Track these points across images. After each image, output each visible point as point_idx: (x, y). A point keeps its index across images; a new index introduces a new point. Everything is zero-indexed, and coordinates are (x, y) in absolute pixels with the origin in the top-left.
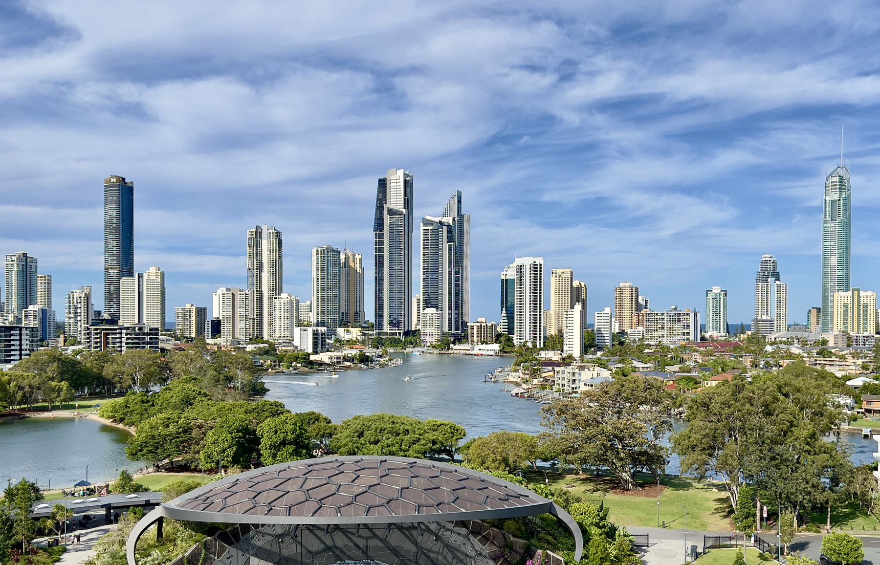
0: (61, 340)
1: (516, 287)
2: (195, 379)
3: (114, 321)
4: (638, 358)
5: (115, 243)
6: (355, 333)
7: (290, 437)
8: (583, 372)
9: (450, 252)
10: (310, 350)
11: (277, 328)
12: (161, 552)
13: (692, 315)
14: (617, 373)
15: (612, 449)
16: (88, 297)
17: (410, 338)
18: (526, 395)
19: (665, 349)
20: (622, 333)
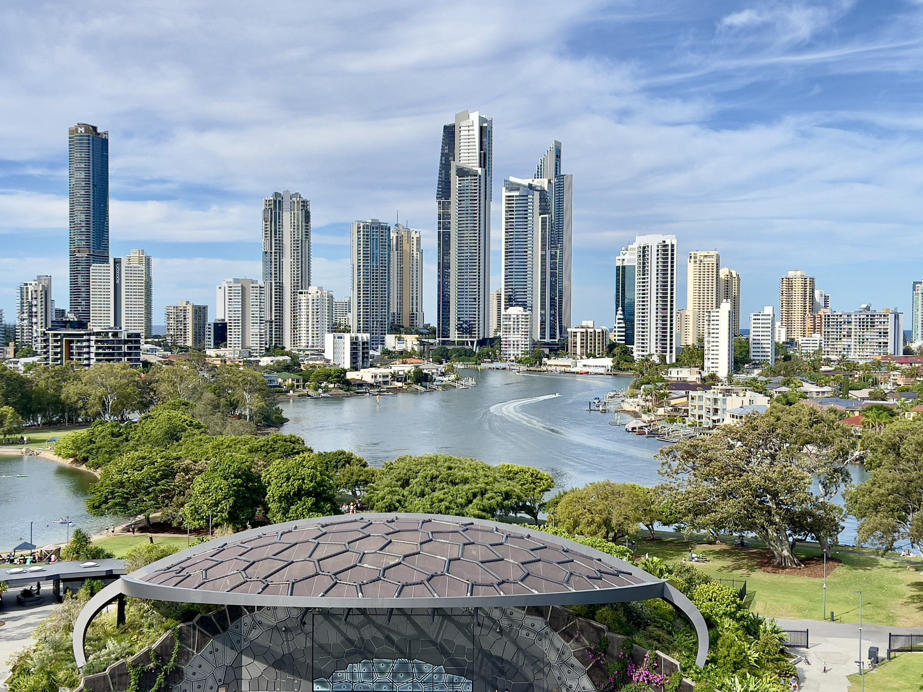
0: (11, 349)
1: (637, 278)
2: (186, 404)
3: (82, 325)
4: (812, 378)
5: (83, 217)
6: (410, 342)
7: (309, 485)
8: (729, 398)
9: (544, 228)
10: (347, 365)
11: (303, 335)
12: (119, 643)
13: (891, 317)
14: (778, 400)
15: (762, 509)
16: (46, 292)
17: (486, 349)
18: (646, 430)
19: (853, 367)
20: (791, 342)
